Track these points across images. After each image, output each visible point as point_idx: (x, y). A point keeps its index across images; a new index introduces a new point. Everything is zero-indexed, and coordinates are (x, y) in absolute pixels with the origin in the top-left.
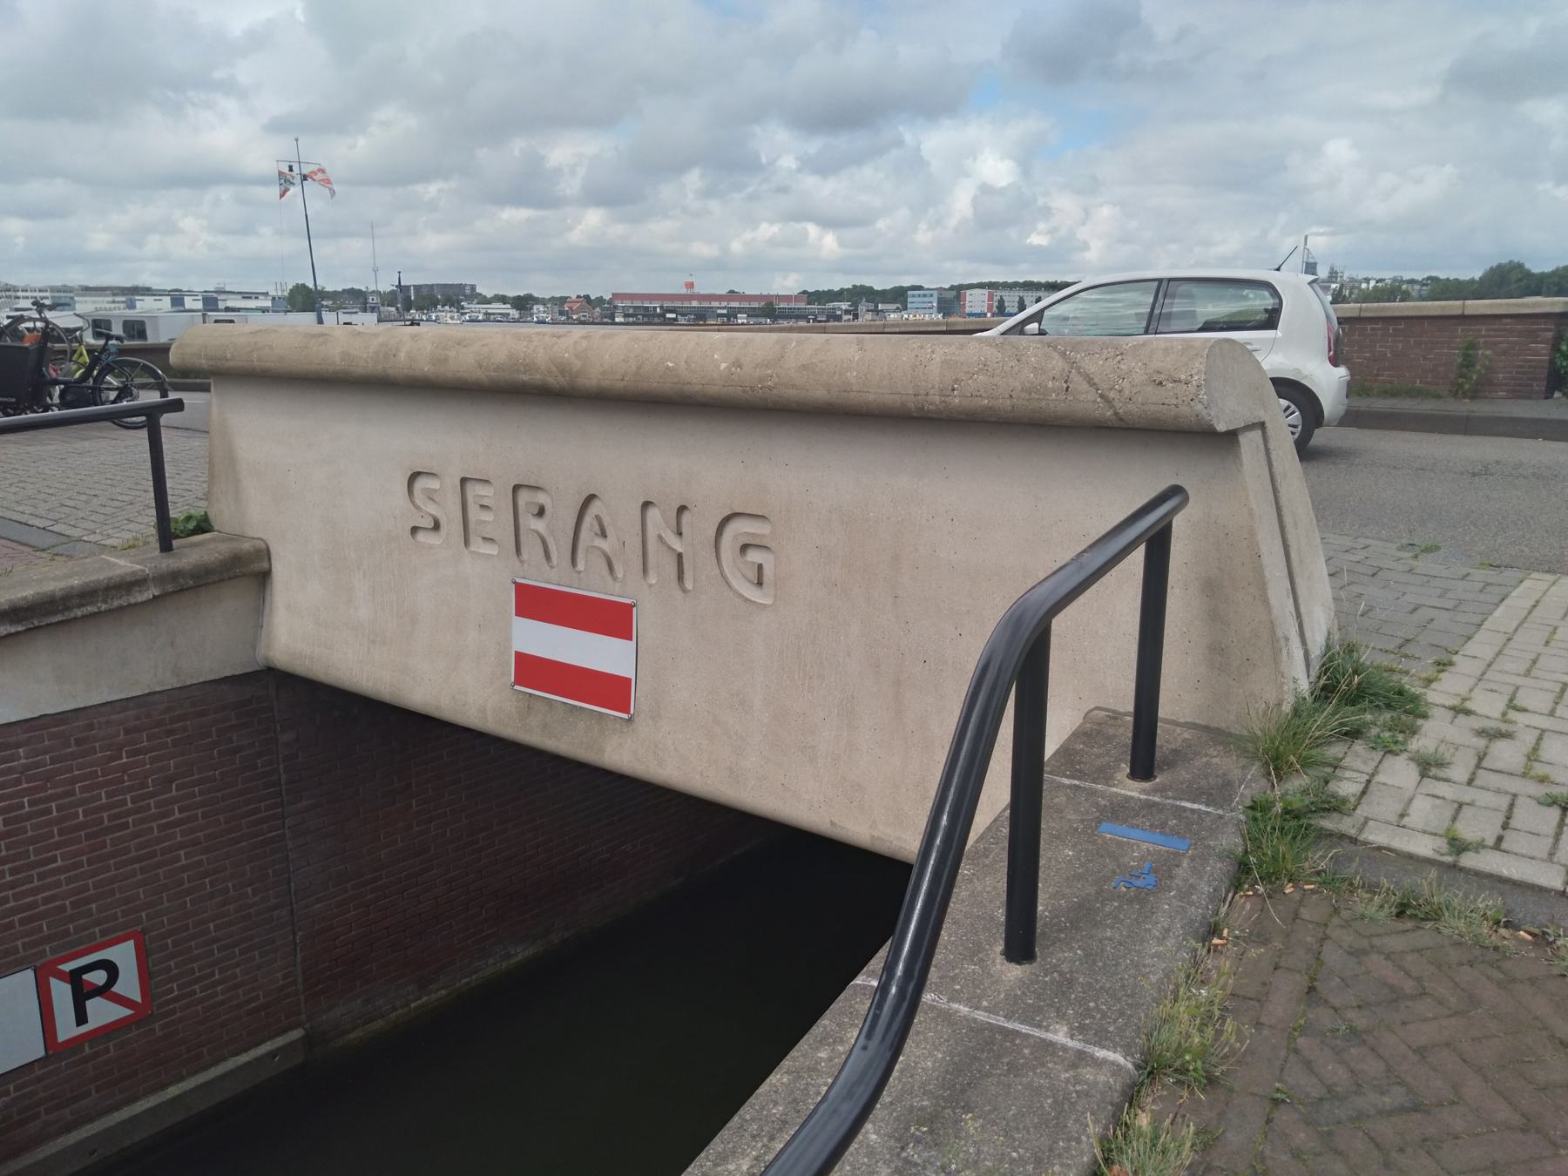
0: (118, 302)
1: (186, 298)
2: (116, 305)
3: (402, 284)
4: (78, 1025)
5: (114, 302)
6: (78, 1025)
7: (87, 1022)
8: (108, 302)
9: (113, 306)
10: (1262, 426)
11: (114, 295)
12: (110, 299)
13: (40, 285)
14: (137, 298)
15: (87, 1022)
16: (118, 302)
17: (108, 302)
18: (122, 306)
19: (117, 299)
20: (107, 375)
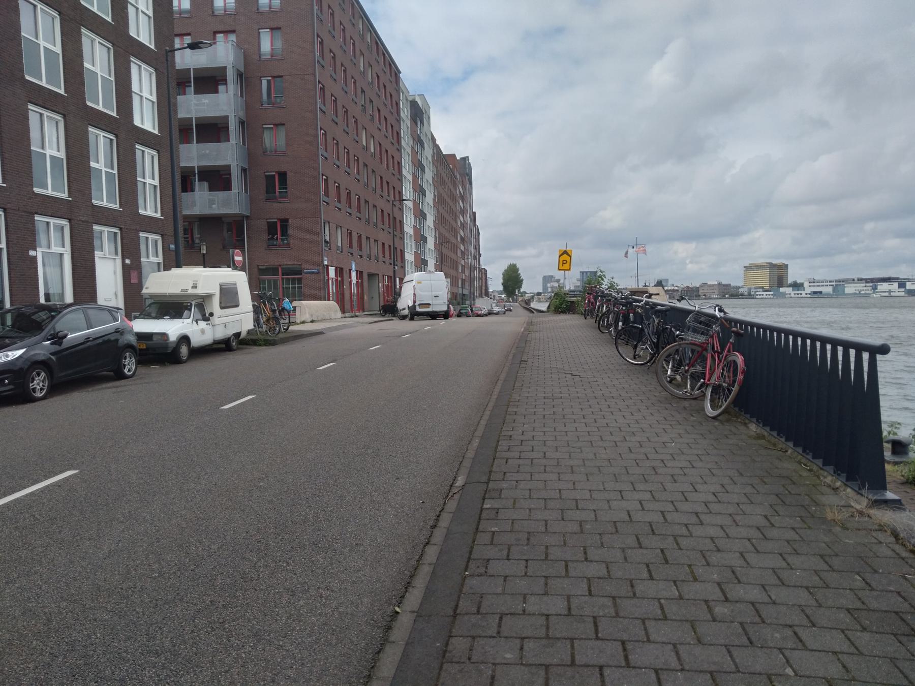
0: (868, 286)
1: (907, 283)
2: (867, 288)
3: (176, 52)
4: (50, 155)
5: (866, 286)
6: (50, 155)
7: (454, 155)
8: (863, 287)
9: (865, 288)
10: (378, 274)
11: (866, 282)
12: (864, 285)
13: (831, 279)
14: (879, 284)
15: (454, 155)
16: (868, 286)
17: (863, 287)
18: (870, 288)
19: (868, 285)
20: (45, 373)
